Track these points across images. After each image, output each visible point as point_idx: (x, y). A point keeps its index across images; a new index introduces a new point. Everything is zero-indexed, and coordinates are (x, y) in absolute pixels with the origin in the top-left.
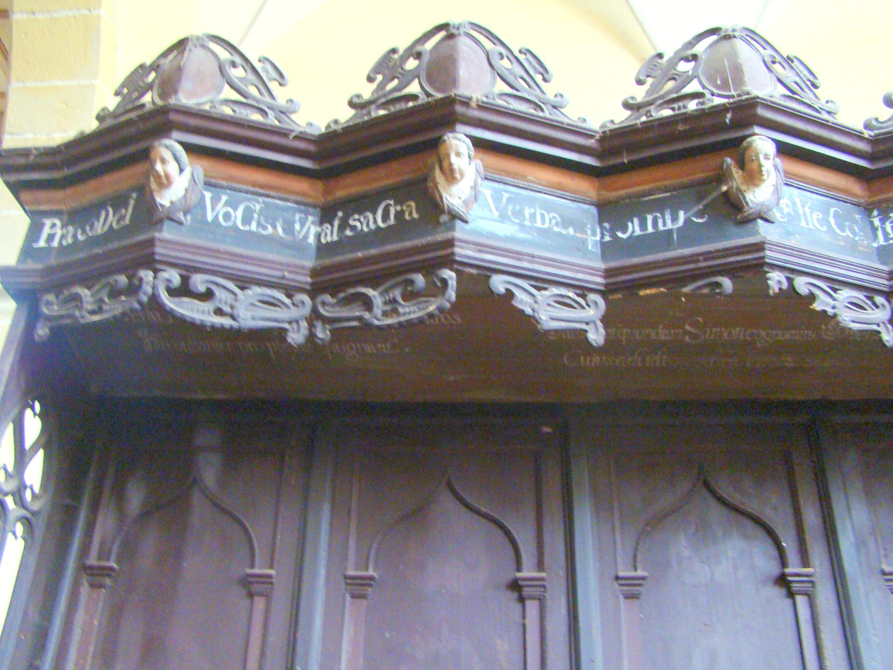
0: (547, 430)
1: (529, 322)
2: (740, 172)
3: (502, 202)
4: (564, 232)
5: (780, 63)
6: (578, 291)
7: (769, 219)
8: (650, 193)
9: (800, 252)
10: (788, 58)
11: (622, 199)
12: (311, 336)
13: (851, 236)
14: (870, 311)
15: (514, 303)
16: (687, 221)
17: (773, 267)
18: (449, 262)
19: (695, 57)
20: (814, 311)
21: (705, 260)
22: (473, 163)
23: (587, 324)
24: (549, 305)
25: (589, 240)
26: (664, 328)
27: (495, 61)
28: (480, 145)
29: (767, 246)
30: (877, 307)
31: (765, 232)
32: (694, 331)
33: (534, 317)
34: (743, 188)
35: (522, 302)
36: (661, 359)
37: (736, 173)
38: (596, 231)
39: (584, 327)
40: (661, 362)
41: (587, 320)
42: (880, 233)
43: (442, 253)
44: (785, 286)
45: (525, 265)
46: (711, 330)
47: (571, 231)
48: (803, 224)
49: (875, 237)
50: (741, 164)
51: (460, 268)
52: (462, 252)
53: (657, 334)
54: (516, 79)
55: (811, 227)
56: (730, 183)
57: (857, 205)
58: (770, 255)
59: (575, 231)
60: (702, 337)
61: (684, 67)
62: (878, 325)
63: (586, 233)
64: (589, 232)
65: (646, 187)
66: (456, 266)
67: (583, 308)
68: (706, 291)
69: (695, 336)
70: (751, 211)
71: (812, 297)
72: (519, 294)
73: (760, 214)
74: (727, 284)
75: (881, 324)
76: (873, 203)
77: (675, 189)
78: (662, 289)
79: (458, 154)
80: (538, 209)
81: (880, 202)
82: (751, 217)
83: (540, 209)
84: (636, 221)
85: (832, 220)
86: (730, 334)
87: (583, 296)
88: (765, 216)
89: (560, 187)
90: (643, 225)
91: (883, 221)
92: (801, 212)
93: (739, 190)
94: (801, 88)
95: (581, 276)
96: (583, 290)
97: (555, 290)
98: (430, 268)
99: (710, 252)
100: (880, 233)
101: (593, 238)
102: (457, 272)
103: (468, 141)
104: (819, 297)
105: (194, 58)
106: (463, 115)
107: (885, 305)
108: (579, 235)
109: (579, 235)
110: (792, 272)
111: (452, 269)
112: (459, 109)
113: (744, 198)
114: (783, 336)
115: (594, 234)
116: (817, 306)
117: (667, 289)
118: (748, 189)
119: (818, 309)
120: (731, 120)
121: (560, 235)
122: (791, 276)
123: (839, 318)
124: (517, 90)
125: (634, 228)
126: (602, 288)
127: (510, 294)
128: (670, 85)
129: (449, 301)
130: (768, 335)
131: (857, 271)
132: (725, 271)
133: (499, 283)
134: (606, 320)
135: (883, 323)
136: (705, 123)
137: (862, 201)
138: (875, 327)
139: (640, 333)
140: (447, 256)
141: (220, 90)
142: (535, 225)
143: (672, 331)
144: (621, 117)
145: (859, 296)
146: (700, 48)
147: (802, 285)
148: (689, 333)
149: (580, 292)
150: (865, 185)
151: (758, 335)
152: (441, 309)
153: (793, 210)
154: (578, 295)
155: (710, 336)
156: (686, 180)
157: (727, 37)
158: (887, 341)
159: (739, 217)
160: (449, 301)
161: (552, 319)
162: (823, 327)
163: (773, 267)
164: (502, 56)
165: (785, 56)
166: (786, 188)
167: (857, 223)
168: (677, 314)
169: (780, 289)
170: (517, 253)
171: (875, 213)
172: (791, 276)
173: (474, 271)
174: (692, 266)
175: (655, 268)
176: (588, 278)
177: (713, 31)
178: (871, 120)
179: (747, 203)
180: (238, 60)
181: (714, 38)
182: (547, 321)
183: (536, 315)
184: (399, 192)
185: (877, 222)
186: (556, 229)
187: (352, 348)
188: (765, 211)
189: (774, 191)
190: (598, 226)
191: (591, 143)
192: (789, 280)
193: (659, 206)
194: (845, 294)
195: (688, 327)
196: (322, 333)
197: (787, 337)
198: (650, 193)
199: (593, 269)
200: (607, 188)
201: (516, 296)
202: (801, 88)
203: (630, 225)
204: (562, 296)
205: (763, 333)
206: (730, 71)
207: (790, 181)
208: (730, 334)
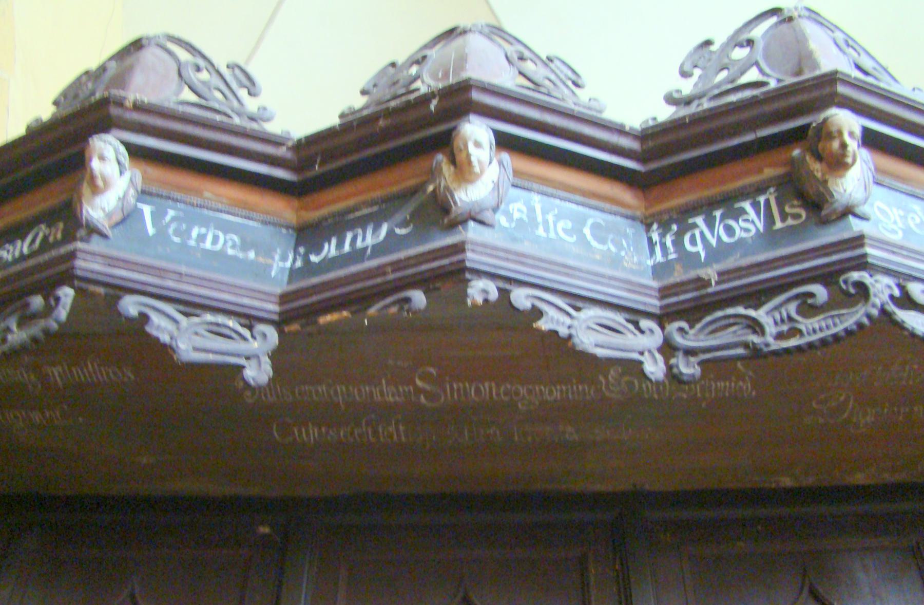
0: (265, 530)
1: (165, 351)
2: (452, 168)
3: (165, 219)
4: (241, 255)
5: (532, 60)
6: (243, 321)
7: (486, 221)
8: (356, 208)
9: (521, 257)
10: (548, 58)
11: (325, 219)
12: (672, 375)
13: (613, 249)
14: (630, 336)
15: (148, 329)
16: (390, 233)
17: (479, 273)
18: (68, 278)
19: (750, 43)
20: (538, 330)
21: (394, 271)
22: (128, 175)
23: (248, 358)
24: (196, 334)
25: (275, 266)
26: (388, 383)
27: (191, 74)
28: (137, 153)
29: (468, 246)
30: (642, 332)
31: (856, 226)
32: (428, 387)
33: (171, 348)
34: (452, 186)
35: (159, 328)
36: (397, 430)
37: (447, 170)
38: (288, 256)
39: (242, 361)
40: (399, 436)
41: (247, 354)
42: (658, 249)
43: (62, 268)
44: (494, 295)
45: (170, 284)
46: (452, 388)
47: (252, 255)
48: (540, 232)
49: (652, 252)
50: (453, 161)
51: (84, 285)
52: (83, 265)
53: (382, 392)
54: (209, 89)
55: (552, 235)
56: (438, 182)
57: (633, 218)
58: (472, 258)
59: (256, 254)
60: (443, 398)
61: (739, 54)
62: (642, 353)
63: (273, 259)
64: (277, 257)
65: (351, 202)
66: (76, 283)
67: (244, 338)
68: (394, 310)
69: (431, 397)
70: (459, 212)
71: (537, 314)
72: (155, 318)
73: (470, 214)
74: (419, 298)
75: (646, 354)
76: (653, 215)
77: (383, 201)
78: (345, 313)
79: (102, 158)
80: (213, 228)
81: (661, 213)
82: (459, 219)
83: (215, 229)
84: (334, 241)
85: (587, 231)
86: (478, 391)
87: (250, 328)
88: (479, 217)
89: (245, 206)
90: (340, 244)
91: (663, 236)
92: (540, 219)
93: (447, 188)
94: (554, 84)
95: (246, 301)
96: (250, 320)
97: (209, 317)
98: (48, 288)
99: (399, 261)
100: (658, 249)
101: (281, 264)
102: (78, 290)
103: (122, 149)
104: (547, 313)
105: (150, 55)
106: (119, 117)
107: (654, 330)
108: (261, 260)
109: (261, 260)
110: (508, 281)
111: (72, 286)
112: (114, 111)
113: (453, 196)
114: (551, 393)
115: (284, 258)
116: (543, 325)
117: (352, 313)
118: (459, 186)
119: (543, 328)
120: (436, 107)
121: (235, 258)
122: (507, 286)
123: (576, 340)
124: (206, 99)
125: (330, 249)
126: (276, 317)
127: (144, 318)
128: (724, 74)
129: (57, 321)
130: (529, 392)
131: (596, 278)
132: (413, 283)
133: (131, 306)
134: (276, 356)
135: (650, 351)
136: (412, 115)
137: (638, 213)
138: (635, 356)
139: (360, 390)
140: (67, 271)
141: (180, 91)
142: (202, 245)
143: (401, 389)
144: (665, 113)
145: (618, 318)
146: (758, 32)
147: (521, 298)
148: (423, 391)
149: (246, 322)
150: (640, 194)
151: (517, 393)
152: (47, 332)
153: (528, 216)
154: (242, 325)
155: (452, 396)
156: (395, 189)
157: (790, 19)
158: (652, 373)
159: (446, 221)
160: (57, 321)
161: (196, 349)
162: (601, 378)
163: (479, 273)
164: (198, 69)
165: (544, 58)
166: (514, 192)
167: (626, 236)
168: (399, 363)
169: (486, 301)
170: (160, 269)
171: (655, 226)
172: (507, 286)
173: (101, 290)
174: (379, 280)
175: (336, 287)
176: (257, 304)
177: (775, 12)
178: (647, 121)
179: (455, 203)
180: (202, 63)
181: (774, 20)
182: (187, 351)
183: (174, 344)
184: (49, 217)
185: (655, 237)
186: (230, 252)
187: (16, 417)
188: (477, 210)
189: (493, 189)
190: (292, 251)
191: (282, 152)
192: (902, 288)
193: (362, 222)
194: (592, 313)
195: (419, 383)
196: (688, 368)
197: (557, 394)
198: (356, 208)
199: (265, 293)
200: (305, 209)
201: (152, 321)
202: (554, 84)
203: (326, 246)
204: (218, 325)
205: (523, 391)
206: (454, 60)
207: (521, 181)
208: (478, 391)
